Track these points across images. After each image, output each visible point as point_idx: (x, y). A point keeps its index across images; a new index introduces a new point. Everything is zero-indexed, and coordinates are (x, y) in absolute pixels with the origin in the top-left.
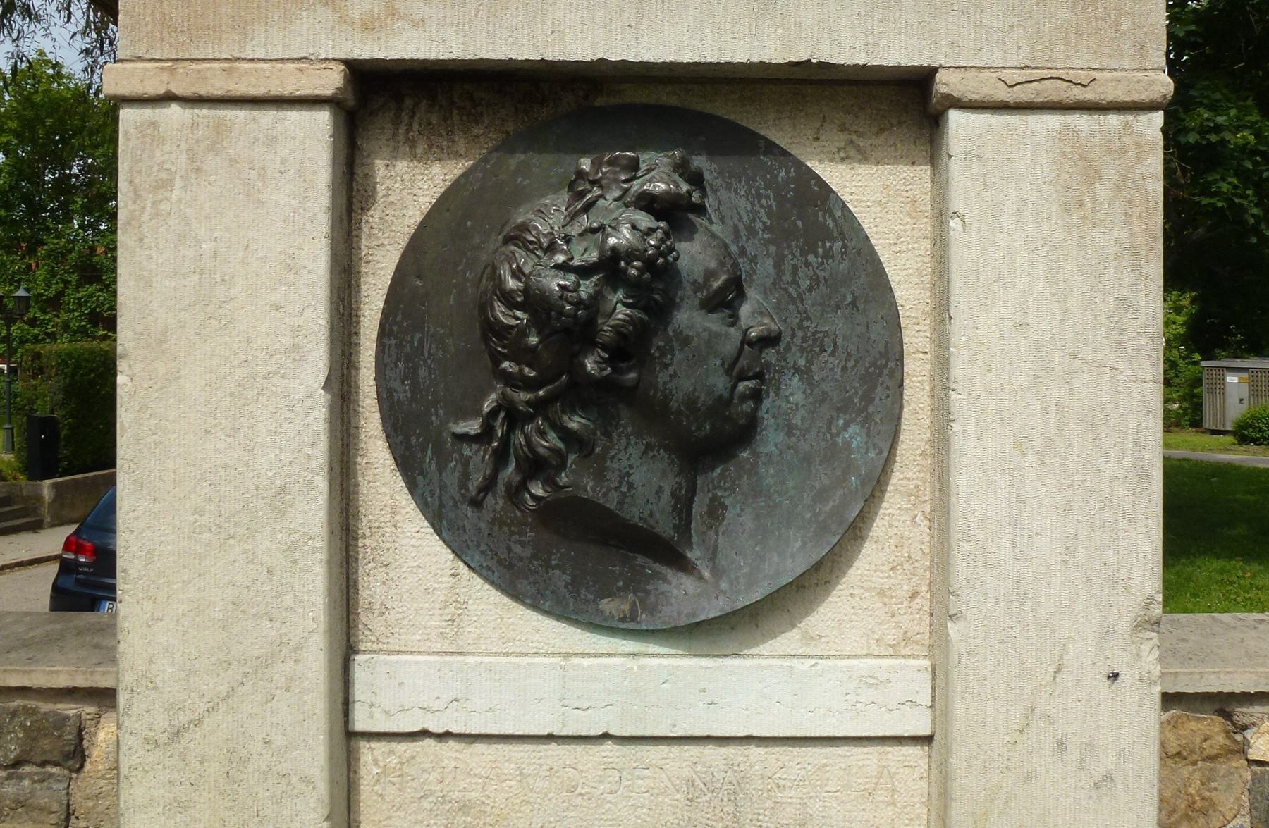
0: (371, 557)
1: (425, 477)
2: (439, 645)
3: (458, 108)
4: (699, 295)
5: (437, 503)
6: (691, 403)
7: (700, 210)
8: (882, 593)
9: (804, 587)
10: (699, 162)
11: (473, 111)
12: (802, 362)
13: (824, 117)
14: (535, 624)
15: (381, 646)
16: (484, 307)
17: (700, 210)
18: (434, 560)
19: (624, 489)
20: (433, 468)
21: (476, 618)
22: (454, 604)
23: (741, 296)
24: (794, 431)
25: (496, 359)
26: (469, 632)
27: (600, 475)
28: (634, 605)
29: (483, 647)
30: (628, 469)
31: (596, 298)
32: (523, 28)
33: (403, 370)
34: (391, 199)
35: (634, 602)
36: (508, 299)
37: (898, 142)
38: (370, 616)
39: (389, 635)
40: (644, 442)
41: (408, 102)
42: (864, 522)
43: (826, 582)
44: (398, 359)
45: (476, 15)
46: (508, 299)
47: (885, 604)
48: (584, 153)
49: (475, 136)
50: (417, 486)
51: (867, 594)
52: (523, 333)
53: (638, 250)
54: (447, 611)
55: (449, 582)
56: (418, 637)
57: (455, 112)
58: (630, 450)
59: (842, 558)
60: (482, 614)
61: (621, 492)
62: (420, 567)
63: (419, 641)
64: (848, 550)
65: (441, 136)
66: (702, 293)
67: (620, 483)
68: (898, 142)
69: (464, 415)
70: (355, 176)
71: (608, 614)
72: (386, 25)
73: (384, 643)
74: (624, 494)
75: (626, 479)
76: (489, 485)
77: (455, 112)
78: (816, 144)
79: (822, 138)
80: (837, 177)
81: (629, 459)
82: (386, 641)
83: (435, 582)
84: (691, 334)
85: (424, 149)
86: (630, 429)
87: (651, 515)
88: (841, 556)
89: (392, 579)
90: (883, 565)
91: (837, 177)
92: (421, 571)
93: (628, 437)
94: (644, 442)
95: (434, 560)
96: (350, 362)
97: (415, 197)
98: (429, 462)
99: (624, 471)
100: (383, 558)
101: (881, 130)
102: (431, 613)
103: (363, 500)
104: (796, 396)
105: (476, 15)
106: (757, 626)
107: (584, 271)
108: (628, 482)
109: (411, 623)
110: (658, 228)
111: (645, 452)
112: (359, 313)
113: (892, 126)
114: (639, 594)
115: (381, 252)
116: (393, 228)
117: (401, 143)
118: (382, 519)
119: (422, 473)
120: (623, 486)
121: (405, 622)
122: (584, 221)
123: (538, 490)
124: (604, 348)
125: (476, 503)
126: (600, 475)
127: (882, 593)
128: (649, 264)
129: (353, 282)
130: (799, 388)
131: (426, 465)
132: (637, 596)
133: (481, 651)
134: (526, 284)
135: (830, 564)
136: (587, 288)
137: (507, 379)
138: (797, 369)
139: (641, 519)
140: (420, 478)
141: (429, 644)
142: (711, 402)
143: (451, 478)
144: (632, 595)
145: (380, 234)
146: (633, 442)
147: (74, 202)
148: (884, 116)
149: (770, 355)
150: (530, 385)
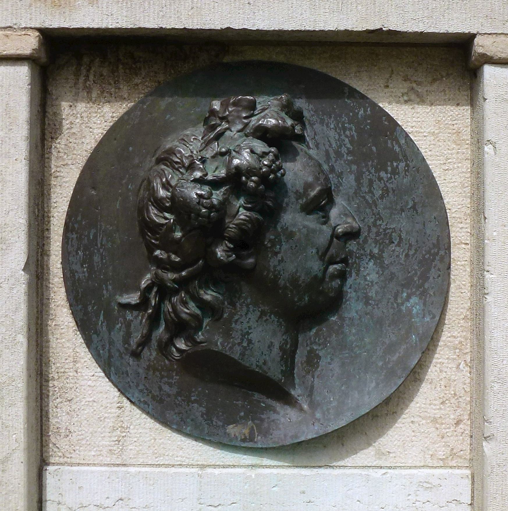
2: (109, 459)
4: (300, 201)
6: (294, 281)
7: (301, 139)
9: (377, 416)
10: (300, 103)
12: (376, 251)
14: (179, 443)
15: (66, 459)
16: (142, 210)
17: (301, 139)
18: (105, 396)
19: (245, 344)
20: (104, 328)
21: (135, 439)
22: (119, 429)
23: (331, 202)
24: (370, 302)
25: (151, 249)
27: (227, 334)
28: (252, 429)
29: (141, 460)
30: (247, 330)
31: (224, 203)
32: (170, 5)
33: (82, 256)
34: (73, 131)
35: (253, 427)
36: (159, 204)
37: (446, 89)
38: (58, 437)
40: (260, 309)
42: (422, 369)
43: (393, 413)
46: (159, 204)
47: (437, 428)
48: (216, 96)
51: (424, 422)
52: (170, 229)
53: (255, 168)
54: (115, 434)
55: (116, 413)
56: (93, 453)
57: (121, 66)
58: (249, 316)
59: (406, 395)
60: (141, 436)
61: (242, 346)
62: (94, 401)
63: (94, 456)
65: (110, 84)
66: (303, 200)
67: (242, 340)
69: (126, 289)
71: (233, 436)
73: (68, 458)
74: (245, 348)
76: (145, 341)
77: (121, 66)
79: (391, 86)
80: (402, 114)
81: (248, 322)
82: (69, 456)
83: (106, 413)
84: (294, 230)
86: (249, 300)
91: (402, 114)
93: (247, 306)
95: (105, 396)
97: (91, 130)
99: (245, 331)
100: (67, 395)
104: (371, 276)
106: (343, 445)
107: (215, 184)
108: (248, 339)
109: (88, 443)
111: (260, 317)
117: (81, 90)
118: (67, 366)
121: (84, 442)
122: (215, 147)
123: (181, 345)
124: (230, 240)
125: (136, 355)
126: (227, 334)
128: (263, 178)
129: (45, 192)
135: (396, 399)
136: (217, 196)
137: (159, 263)
138: (372, 256)
139: (257, 366)
140: (95, 336)
143: (118, 336)
146: (251, 310)
149: (352, 246)
150: (175, 268)
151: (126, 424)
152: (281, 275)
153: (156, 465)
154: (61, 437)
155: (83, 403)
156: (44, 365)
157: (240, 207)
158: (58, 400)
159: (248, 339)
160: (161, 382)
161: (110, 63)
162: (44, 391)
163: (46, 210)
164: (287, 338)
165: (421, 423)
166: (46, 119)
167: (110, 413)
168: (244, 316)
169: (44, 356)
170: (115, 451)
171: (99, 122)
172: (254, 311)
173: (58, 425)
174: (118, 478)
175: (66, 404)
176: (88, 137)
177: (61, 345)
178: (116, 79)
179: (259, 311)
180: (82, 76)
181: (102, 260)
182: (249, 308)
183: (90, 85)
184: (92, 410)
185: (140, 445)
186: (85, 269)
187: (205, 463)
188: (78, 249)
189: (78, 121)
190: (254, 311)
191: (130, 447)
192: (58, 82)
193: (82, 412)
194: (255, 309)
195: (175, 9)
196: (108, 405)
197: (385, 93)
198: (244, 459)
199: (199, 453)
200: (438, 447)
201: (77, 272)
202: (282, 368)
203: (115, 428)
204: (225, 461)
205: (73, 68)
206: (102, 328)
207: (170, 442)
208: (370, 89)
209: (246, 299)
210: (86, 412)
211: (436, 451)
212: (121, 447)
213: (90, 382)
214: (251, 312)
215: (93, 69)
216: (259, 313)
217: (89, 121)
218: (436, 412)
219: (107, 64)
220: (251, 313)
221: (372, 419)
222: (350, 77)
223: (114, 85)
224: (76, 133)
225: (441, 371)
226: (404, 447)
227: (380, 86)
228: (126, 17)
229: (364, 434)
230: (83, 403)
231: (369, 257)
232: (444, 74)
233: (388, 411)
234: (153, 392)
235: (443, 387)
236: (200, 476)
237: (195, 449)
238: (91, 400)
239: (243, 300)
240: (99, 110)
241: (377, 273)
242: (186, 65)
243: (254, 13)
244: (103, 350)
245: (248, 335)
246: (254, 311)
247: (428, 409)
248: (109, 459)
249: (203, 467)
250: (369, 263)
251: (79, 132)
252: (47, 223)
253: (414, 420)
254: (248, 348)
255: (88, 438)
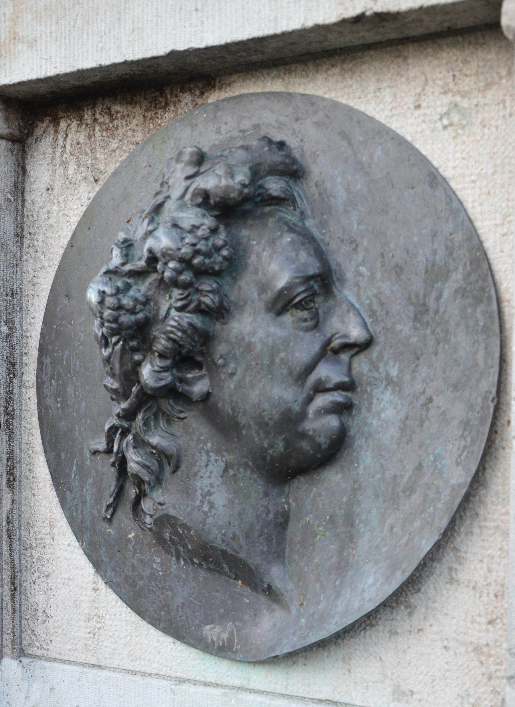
0: (36, 567)
1: (71, 492)
2: (84, 656)
3: (100, 124)
4: (264, 296)
5: (80, 517)
8: (477, 650)
9: (396, 633)
11: (111, 125)
12: (394, 372)
13: (426, 80)
14: (156, 644)
15: (42, 652)
18: (80, 573)
19: (206, 508)
20: (77, 483)
21: (111, 634)
22: (95, 618)
24: (383, 453)
26: (106, 646)
28: (232, 634)
29: (116, 663)
30: (209, 488)
32: (110, 32)
33: (55, 387)
34: (51, 222)
35: (233, 631)
37: (507, 98)
38: (36, 622)
39: (49, 642)
40: (224, 459)
41: (63, 125)
42: (461, 564)
43: (420, 630)
44: (52, 378)
45: (74, 27)
47: (482, 663)
49: (112, 151)
50: (66, 500)
51: (462, 649)
53: (171, 249)
54: (90, 624)
55: (91, 596)
56: (69, 647)
57: (97, 128)
58: (210, 467)
59: (437, 605)
60: (116, 631)
61: (203, 511)
62: (70, 580)
63: (70, 650)
64: (442, 595)
65: (87, 154)
66: (267, 294)
67: (202, 502)
68: (507, 98)
70: (26, 203)
71: (210, 641)
72: (10, 51)
73: (45, 649)
74: (205, 513)
75: (208, 498)
77: (97, 128)
78: (417, 113)
79: (424, 105)
80: (439, 149)
81: (210, 477)
82: (46, 647)
83: (81, 595)
84: (253, 340)
85: (74, 169)
86: (209, 445)
87: (234, 538)
88: (434, 602)
89: (51, 589)
90: (479, 615)
91: (439, 149)
92: (71, 583)
93: (207, 453)
94: (224, 459)
95: (80, 573)
96: (21, 381)
97: (68, 218)
98: (74, 477)
99: (206, 490)
100: (44, 568)
101: (488, 86)
102: (78, 625)
103: (447, 560)
104: (387, 412)
105: (74, 27)
106: (349, 671)
108: (209, 502)
109: (64, 632)
110: (202, 224)
111: (225, 470)
112: (28, 334)
113: (501, 78)
114: (238, 624)
115: (43, 274)
116: (52, 250)
117: (58, 166)
118: (44, 531)
119: (69, 489)
120: (204, 506)
121: (60, 631)
124: (162, 356)
127: (477, 650)
129: (24, 305)
130: (391, 402)
131: (72, 480)
132: (235, 625)
133: (114, 666)
134: (221, 302)
135: (423, 610)
138: (389, 380)
139: (223, 541)
140: (68, 493)
141: (77, 654)
142: (278, 416)
144: (231, 623)
145: (43, 257)
146: (212, 459)
147: (174, 270)
148: (491, 68)
151: (101, 612)
152: (240, 408)
153: (132, 671)
154: (39, 622)
155: (59, 581)
156: (23, 528)
157: (169, 309)
158: (37, 574)
159: (209, 502)
160: (133, 558)
161: (87, 125)
162: (22, 562)
163: (24, 328)
164: (269, 504)
165: (459, 651)
166: (25, 209)
167: (85, 595)
168: (204, 468)
169: (22, 516)
170: (90, 646)
171: (75, 207)
172: (216, 461)
173: (35, 607)
174: (88, 682)
175: (42, 579)
176: (64, 228)
177: (38, 504)
178: (93, 146)
179: (222, 461)
180: (59, 147)
181: (75, 391)
182: (210, 457)
183: (66, 158)
184: (68, 590)
185: (116, 642)
186: (59, 405)
187: (185, 676)
188: (52, 378)
189: (55, 208)
190: (216, 462)
191: (105, 644)
192: (36, 160)
193: (58, 591)
194: (217, 458)
195: (114, 36)
196: (84, 585)
197: (416, 118)
198: (227, 676)
199: (178, 661)
200: (483, 693)
201: (50, 408)
202: (262, 548)
203: (91, 617)
204: (207, 675)
205: (51, 139)
206: (75, 481)
207: (146, 641)
208: (393, 115)
209: (205, 444)
210: (62, 592)
211: (480, 699)
212: (96, 643)
213: (66, 553)
214: (213, 462)
215: (70, 136)
216: (223, 465)
217: (65, 207)
218: (480, 635)
219: (84, 126)
220: (213, 465)
221: (390, 637)
222: (366, 99)
223: (90, 154)
224: (53, 224)
225: (490, 570)
226: (433, 687)
227: (409, 108)
228: (65, 58)
229: (378, 658)
230: (59, 581)
231: (384, 382)
232: (504, 73)
233: (411, 626)
234: (126, 571)
235: (492, 596)
236: (173, 692)
237: (174, 655)
238: (67, 576)
239: (201, 445)
240: (76, 191)
241: (395, 408)
242: (166, 115)
243: (202, 22)
244: (76, 512)
245: (210, 496)
246: (216, 462)
247: (469, 629)
248: (84, 656)
249: (181, 681)
250: (385, 392)
251: (56, 223)
252: (25, 345)
253: (448, 645)
254: (209, 514)
255: (64, 627)
